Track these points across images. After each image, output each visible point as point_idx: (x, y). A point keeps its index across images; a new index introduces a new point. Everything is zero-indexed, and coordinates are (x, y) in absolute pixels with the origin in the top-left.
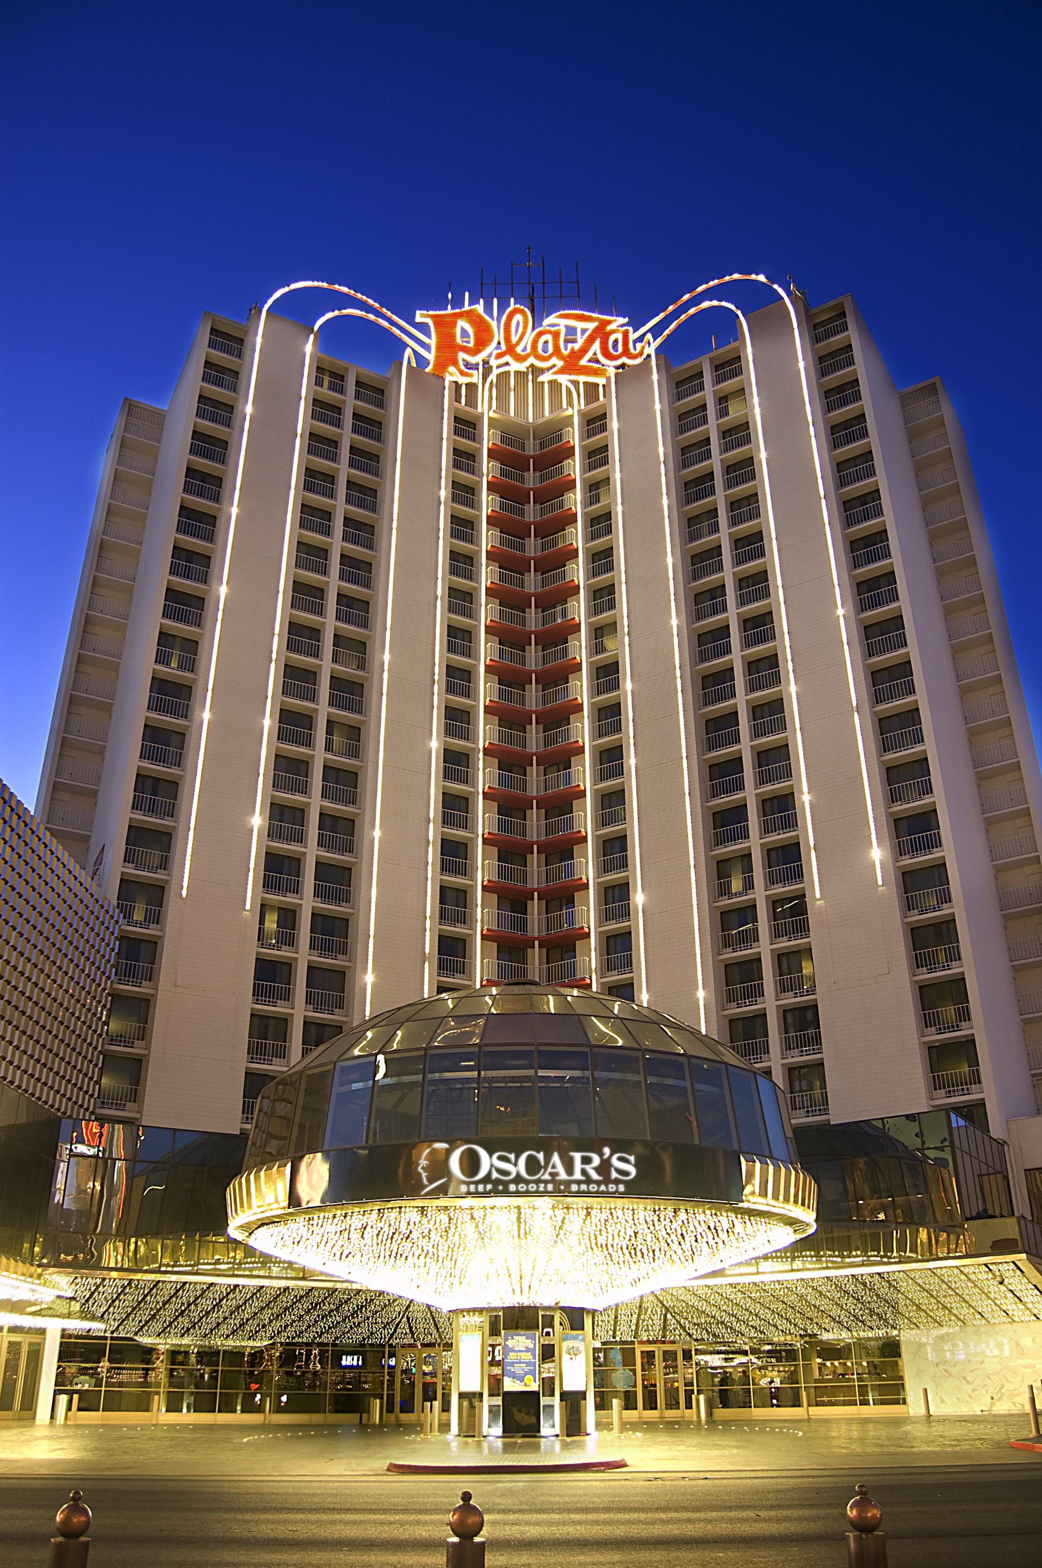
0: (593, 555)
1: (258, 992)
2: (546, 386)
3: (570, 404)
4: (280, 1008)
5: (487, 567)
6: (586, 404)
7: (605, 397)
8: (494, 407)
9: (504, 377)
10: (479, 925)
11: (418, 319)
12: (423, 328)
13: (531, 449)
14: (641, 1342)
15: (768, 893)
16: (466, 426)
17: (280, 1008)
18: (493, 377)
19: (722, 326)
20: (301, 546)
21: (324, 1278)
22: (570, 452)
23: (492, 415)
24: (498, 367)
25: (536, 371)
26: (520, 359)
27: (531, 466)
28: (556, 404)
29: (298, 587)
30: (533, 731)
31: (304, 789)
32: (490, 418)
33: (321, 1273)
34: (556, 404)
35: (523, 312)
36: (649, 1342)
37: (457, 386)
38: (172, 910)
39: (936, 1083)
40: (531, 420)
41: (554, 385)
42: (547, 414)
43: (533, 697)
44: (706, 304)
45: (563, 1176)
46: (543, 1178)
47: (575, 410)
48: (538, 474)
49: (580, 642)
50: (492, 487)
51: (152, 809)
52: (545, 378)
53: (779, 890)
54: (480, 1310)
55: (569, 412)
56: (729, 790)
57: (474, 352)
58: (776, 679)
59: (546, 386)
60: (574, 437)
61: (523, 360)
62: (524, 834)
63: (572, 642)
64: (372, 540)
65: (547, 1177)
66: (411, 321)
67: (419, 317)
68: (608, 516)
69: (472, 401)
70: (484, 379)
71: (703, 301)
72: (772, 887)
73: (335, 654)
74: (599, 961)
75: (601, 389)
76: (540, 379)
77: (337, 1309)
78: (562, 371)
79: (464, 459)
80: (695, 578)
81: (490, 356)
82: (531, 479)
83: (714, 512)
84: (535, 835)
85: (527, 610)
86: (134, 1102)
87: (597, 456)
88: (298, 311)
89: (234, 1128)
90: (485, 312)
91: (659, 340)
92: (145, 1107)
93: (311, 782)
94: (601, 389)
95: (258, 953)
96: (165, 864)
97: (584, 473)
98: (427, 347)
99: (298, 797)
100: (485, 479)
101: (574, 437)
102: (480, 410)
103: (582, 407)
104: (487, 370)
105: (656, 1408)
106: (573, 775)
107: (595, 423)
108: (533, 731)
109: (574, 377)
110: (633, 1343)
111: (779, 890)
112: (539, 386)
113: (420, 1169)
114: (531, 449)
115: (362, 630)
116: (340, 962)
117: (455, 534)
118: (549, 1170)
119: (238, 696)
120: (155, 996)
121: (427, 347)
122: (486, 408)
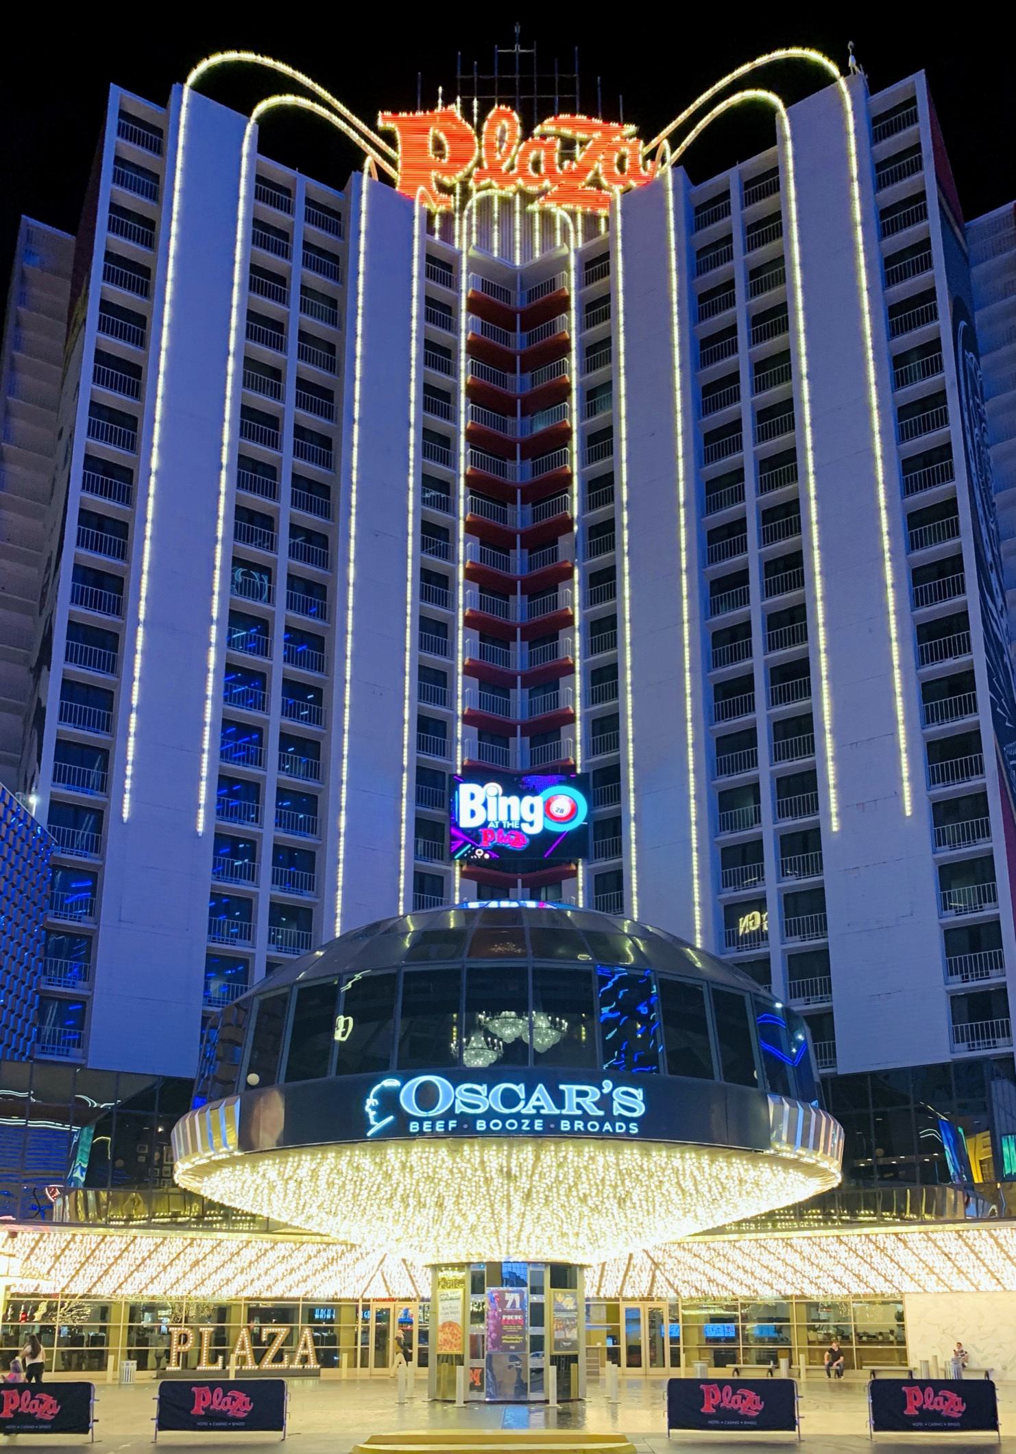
0: (591, 575)
1: (214, 930)
2: (537, 216)
3: (565, 238)
4: (242, 888)
5: (465, 544)
6: (585, 240)
7: (607, 229)
8: (474, 241)
9: (485, 204)
10: (460, 655)
11: (380, 123)
12: (389, 137)
13: (518, 302)
14: (625, 1299)
15: (781, 885)
16: (441, 268)
17: (242, 888)
18: (472, 203)
19: (752, 130)
20: (249, 364)
21: (290, 1230)
22: (562, 304)
23: (472, 252)
24: (478, 190)
25: (528, 198)
26: (505, 180)
27: (519, 319)
28: (548, 243)
29: (236, 618)
30: (518, 602)
31: (258, 760)
32: (469, 258)
33: (286, 1225)
34: (548, 243)
35: (509, 117)
36: (633, 1299)
37: (430, 217)
38: (112, 838)
39: (957, 1037)
40: (518, 263)
41: (547, 217)
42: (537, 254)
43: (518, 654)
44: (736, 99)
45: (550, 1109)
46: (523, 1111)
47: (572, 246)
48: (529, 462)
49: (574, 689)
50: (467, 719)
51: (82, 783)
52: (534, 207)
53: (789, 823)
54: (461, 1266)
55: (565, 251)
56: (735, 657)
57: (448, 171)
58: (806, 690)
59: (537, 216)
60: (571, 284)
61: (510, 183)
62: (508, 664)
63: (563, 588)
64: (321, 658)
65: (529, 1110)
66: (372, 125)
67: (385, 120)
68: (606, 299)
69: (447, 234)
70: (462, 207)
71: (730, 93)
72: (790, 939)
73: (282, 760)
74: (583, 643)
75: (603, 221)
76: (530, 207)
77: (310, 1258)
78: (559, 199)
79: (439, 312)
80: (712, 561)
81: (469, 176)
82: (518, 341)
83: (739, 474)
84: (519, 523)
85: (511, 597)
86: (79, 1046)
87: (596, 310)
88: (233, 89)
89: (192, 1074)
90: (463, 116)
91: (678, 152)
92: (96, 984)
93: (263, 808)
94: (603, 221)
95: (213, 887)
96: (103, 786)
97: (587, 758)
98: (392, 162)
99: (255, 713)
100: (461, 566)
101: (571, 284)
102: (457, 246)
103: (580, 245)
104: (466, 193)
105: (639, 1365)
106: (560, 647)
107: (596, 266)
108: (518, 695)
109: (569, 206)
110: (617, 1299)
111: (789, 823)
112: (528, 218)
113: (367, 1109)
114: (518, 302)
115: (316, 675)
116: (304, 898)
117: (425, 595)
118: (533, 1102)
119: (179, 634)
120: (96, 931)
121: (392, 162)
122: (464, 244)
